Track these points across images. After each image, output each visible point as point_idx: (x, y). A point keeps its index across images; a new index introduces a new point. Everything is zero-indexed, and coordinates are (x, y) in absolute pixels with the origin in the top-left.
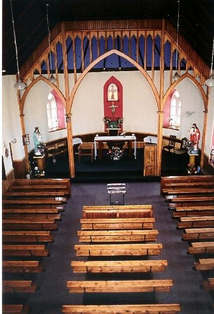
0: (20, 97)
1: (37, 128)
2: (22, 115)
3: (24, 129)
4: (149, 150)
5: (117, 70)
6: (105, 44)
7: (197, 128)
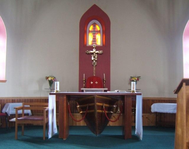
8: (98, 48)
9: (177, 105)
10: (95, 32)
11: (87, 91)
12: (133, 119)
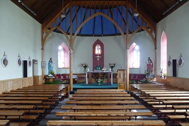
1: (51, 59)
2: (42, 49)
7: (150, 60)
8: (100, 55)
10: (98, 49)
11: (96, 71)
12: (134, 82)
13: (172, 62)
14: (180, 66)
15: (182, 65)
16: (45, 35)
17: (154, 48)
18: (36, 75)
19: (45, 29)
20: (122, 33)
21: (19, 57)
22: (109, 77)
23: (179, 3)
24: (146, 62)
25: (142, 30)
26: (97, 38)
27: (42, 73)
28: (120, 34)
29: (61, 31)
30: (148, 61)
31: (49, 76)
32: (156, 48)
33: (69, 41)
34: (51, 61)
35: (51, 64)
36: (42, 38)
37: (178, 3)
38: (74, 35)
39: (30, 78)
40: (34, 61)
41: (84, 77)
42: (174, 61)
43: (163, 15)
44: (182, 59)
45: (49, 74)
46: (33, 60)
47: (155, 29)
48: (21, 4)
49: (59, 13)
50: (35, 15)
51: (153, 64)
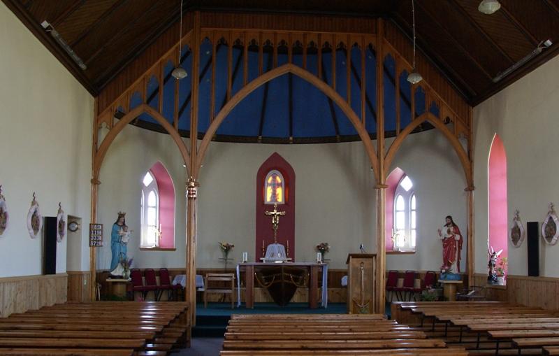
0: (96, 143)
1: (121, 216)
2: (95, 182)
3: (94, 211)
4: (357, 265)
5: (286, 142)
6: (272, 54)
7: (454, 225)
8: (280, 208)
9: (550, 46)
10: (275, 186)
13: (524, 229)
14: (550, 241)
15: (555, 238)
16: (103, 134)
17: (464, 186)
18: (75, 269)
19: (107, 116)
20: (364, 135)
21: (34, 203)
22: (315, 281)
23: (544, 50)
24: (439, 231)
25: (426, 126)
26: (270, 149)
27: (93, 264)
28: (357, 138)
29: (161, 126)
30: (446, 228)
31: (112, 273)
32: (470, 187)
33: (187, 157)
34: (121, 221)
35: (122, 232)
36: (95, 143)
37: (540, 49)
38: (202, 139)
39: (61, 276)
40: (73, 220)
41: (230, 281)
42: (533, 227)
43: (496, 84)
44: (555, 219)
45: (113, 267)
46: (69, 217)
47: (468, 125)
48: (49, 34)
49: (157, 63)
50: (83, 67)
51: (461, 238)
